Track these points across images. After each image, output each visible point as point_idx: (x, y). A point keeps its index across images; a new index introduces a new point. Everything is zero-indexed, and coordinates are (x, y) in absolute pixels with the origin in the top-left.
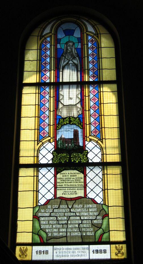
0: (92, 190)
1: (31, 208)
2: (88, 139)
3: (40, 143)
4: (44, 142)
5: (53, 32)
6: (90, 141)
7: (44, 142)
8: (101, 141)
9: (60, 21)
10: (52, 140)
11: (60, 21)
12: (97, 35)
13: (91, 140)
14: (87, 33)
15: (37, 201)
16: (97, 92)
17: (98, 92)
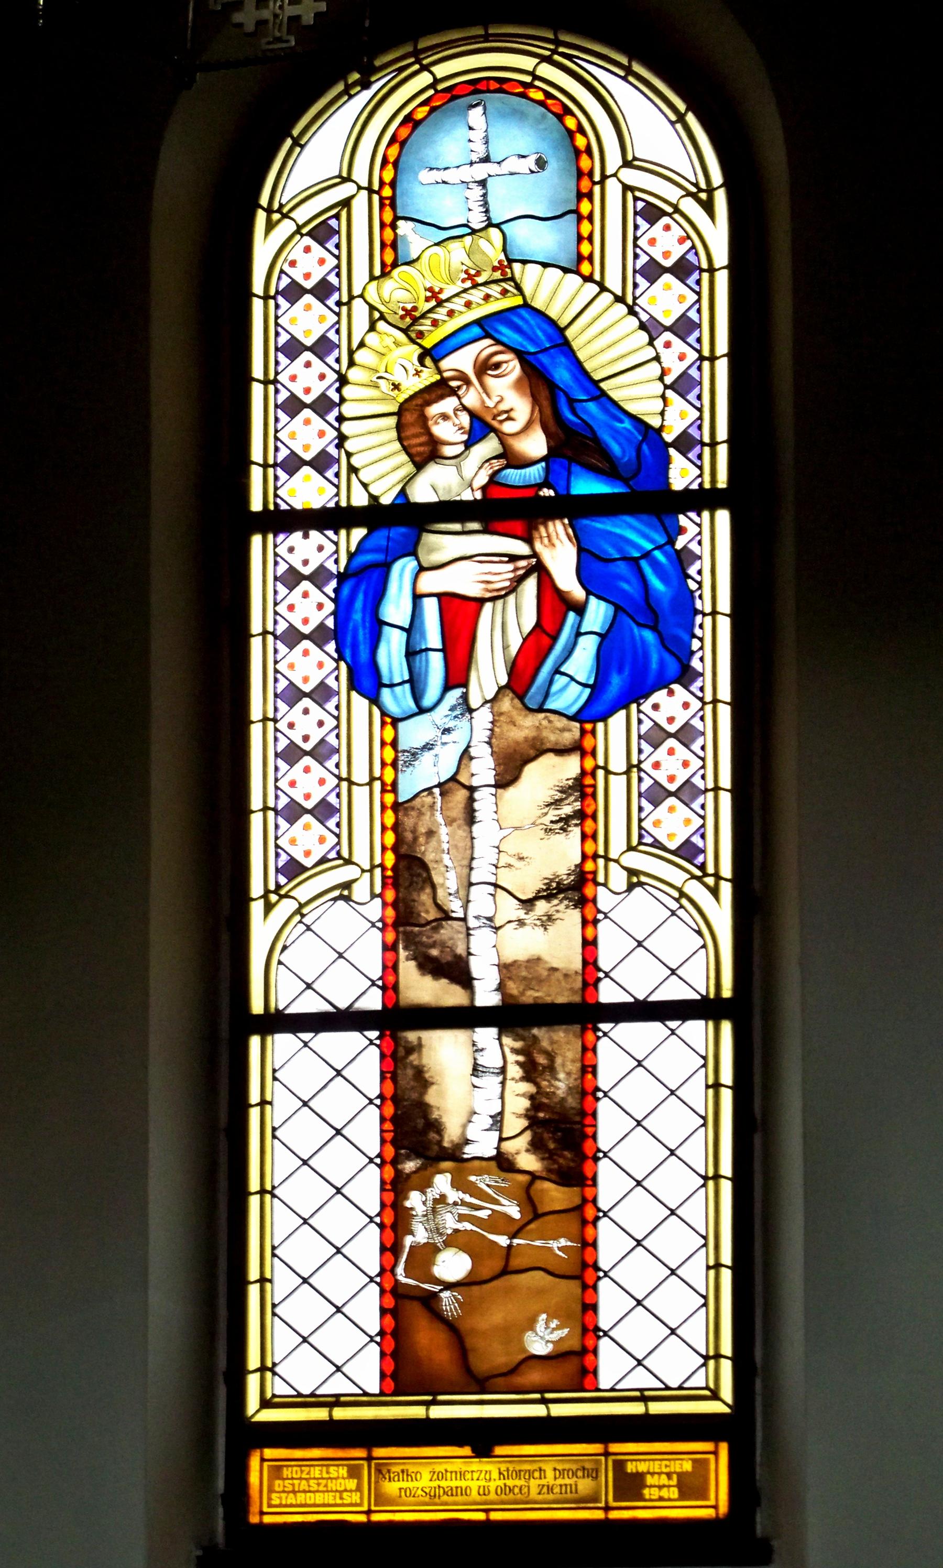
0: (639, 1243)
2: (618, 879)
3: (279, 221)
6: (631, 887)
8: (699, 201)
9: (425, 79)
10: (361, 891)
11: (425, 79)
13: (635, 880)
14: (631, 177)
15: (365, 1399)
16: (696, 355)
17: (702, 358)
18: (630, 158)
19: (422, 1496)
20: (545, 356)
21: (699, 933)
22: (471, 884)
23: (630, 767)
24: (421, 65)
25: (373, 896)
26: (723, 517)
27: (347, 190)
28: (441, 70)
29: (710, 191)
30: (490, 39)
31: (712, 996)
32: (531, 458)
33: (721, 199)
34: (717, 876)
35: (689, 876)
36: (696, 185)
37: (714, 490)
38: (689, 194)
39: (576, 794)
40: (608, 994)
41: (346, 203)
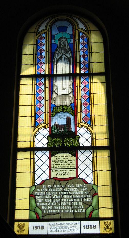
0: (83, 171)
2: (80, 126)
3: (36, 129)
4: (39, 128)
5: (48, 29)
6: (81, 127)
7: (39, 128)
8: (91, 127)
9: (54, 19)
10: (47, 127)
11: (54, 19)
12: (87, 32)
13: (82, 126)
14: (78, 30)
15: (34, 181)
16: (88, 83)
17: (89, 83)
20: (24, 72)
22: (60, 181)
32: (24, 49)
39: (43, 28)
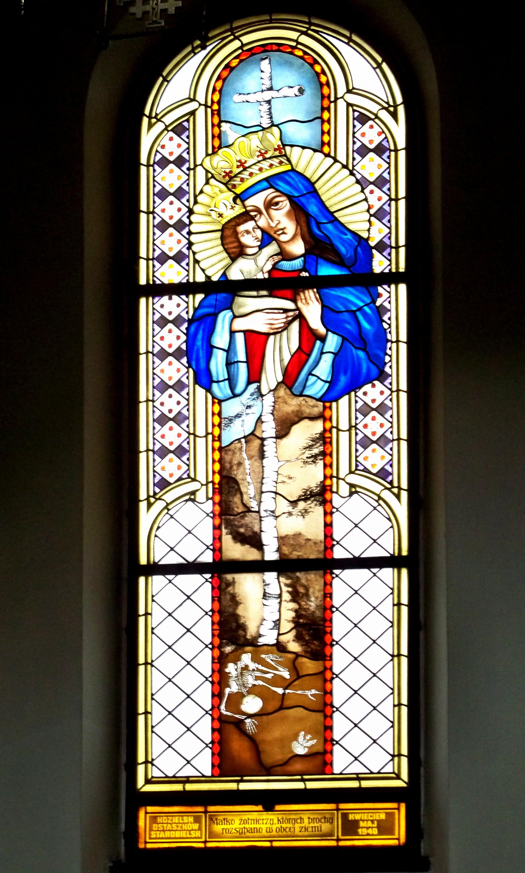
0: (356, 692)
1: (160, 347)
2: (344, 489)
3: (155, 123)
6: (351, 494)
8: (389, 112)
9: (237, 44)
10: (201, 496)
11: (237, 44)
13: (354, 490)
14: (351, 98)
15: (203, 779)
16: (388, 198)
17: (391, 199)
18: (351, 88)
19: (235, 833)
21: (389, 519)
23: (351, 427)
24: (234, 36)
25: (208, 499)
26: (403, 288)
27: (193, 106)
28: (246, 39)
29: (395, 106)
30: (273, 21)
31: (396, 554)
33: (401, 111)
34: (399, 488)
35: (384, 488)
36: (387, 103)
37: (397, 273)
38: (384, 108)
40: (338, 553)
41: (193, 113)
